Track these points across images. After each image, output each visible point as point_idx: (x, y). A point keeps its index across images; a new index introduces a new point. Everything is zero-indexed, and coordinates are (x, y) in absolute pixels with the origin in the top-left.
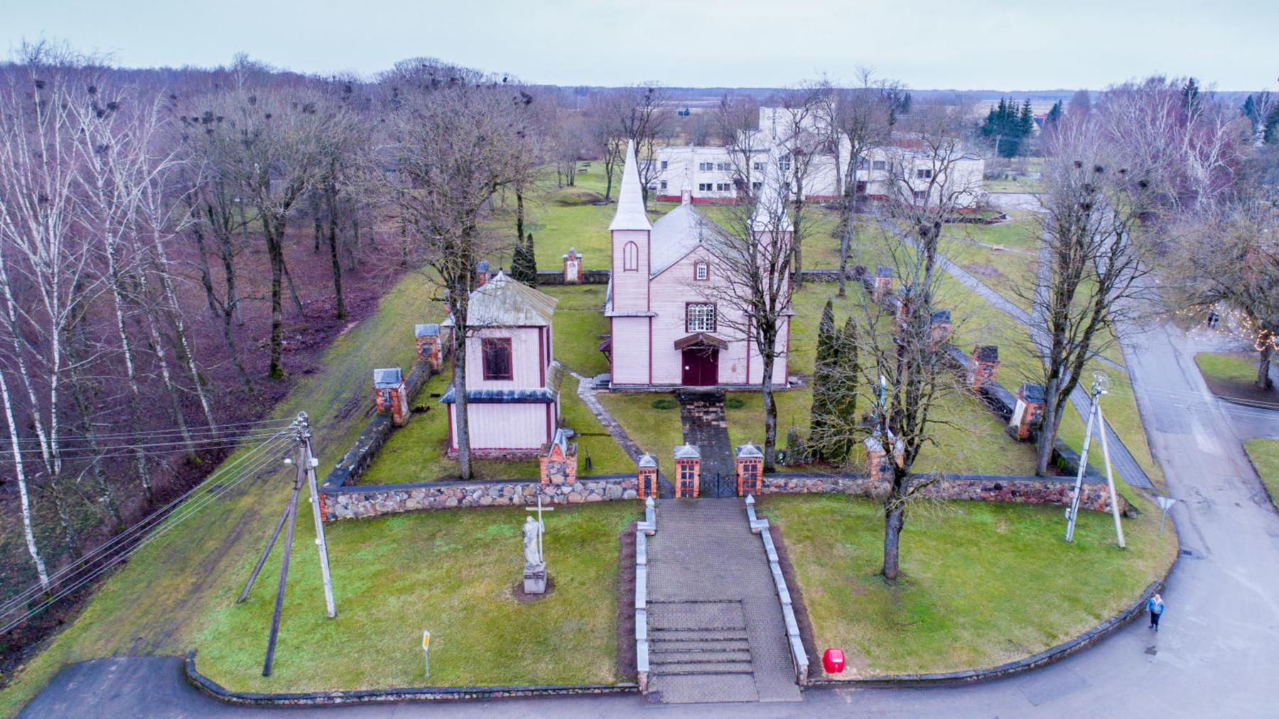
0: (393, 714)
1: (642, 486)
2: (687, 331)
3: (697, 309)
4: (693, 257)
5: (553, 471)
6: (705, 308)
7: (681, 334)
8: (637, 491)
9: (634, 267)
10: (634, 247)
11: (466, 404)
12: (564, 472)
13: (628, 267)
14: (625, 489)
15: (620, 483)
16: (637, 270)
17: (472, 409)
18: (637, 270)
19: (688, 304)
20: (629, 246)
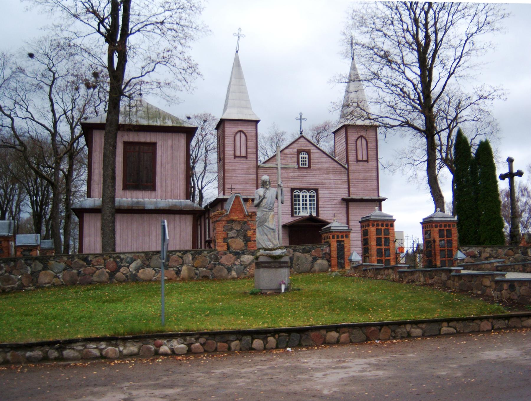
0: (94, 206)
1: (334, 254)
2: (292, 216)
3: (301, 194)
4: (296, 147)
5: (232, 234)
6: (308, 194)
7: (288, 219)
8: (329, 261)
9: (244, 154)
10: (243, 136)
11: (113, 216)
12: (245, 236)
13: (238, 154)
14: (315, 259)
15: (308, 252)
16: (246, 157)
17: (118, 217)
18: (246, 157)
19: (292, 190)
20: (238, 135)
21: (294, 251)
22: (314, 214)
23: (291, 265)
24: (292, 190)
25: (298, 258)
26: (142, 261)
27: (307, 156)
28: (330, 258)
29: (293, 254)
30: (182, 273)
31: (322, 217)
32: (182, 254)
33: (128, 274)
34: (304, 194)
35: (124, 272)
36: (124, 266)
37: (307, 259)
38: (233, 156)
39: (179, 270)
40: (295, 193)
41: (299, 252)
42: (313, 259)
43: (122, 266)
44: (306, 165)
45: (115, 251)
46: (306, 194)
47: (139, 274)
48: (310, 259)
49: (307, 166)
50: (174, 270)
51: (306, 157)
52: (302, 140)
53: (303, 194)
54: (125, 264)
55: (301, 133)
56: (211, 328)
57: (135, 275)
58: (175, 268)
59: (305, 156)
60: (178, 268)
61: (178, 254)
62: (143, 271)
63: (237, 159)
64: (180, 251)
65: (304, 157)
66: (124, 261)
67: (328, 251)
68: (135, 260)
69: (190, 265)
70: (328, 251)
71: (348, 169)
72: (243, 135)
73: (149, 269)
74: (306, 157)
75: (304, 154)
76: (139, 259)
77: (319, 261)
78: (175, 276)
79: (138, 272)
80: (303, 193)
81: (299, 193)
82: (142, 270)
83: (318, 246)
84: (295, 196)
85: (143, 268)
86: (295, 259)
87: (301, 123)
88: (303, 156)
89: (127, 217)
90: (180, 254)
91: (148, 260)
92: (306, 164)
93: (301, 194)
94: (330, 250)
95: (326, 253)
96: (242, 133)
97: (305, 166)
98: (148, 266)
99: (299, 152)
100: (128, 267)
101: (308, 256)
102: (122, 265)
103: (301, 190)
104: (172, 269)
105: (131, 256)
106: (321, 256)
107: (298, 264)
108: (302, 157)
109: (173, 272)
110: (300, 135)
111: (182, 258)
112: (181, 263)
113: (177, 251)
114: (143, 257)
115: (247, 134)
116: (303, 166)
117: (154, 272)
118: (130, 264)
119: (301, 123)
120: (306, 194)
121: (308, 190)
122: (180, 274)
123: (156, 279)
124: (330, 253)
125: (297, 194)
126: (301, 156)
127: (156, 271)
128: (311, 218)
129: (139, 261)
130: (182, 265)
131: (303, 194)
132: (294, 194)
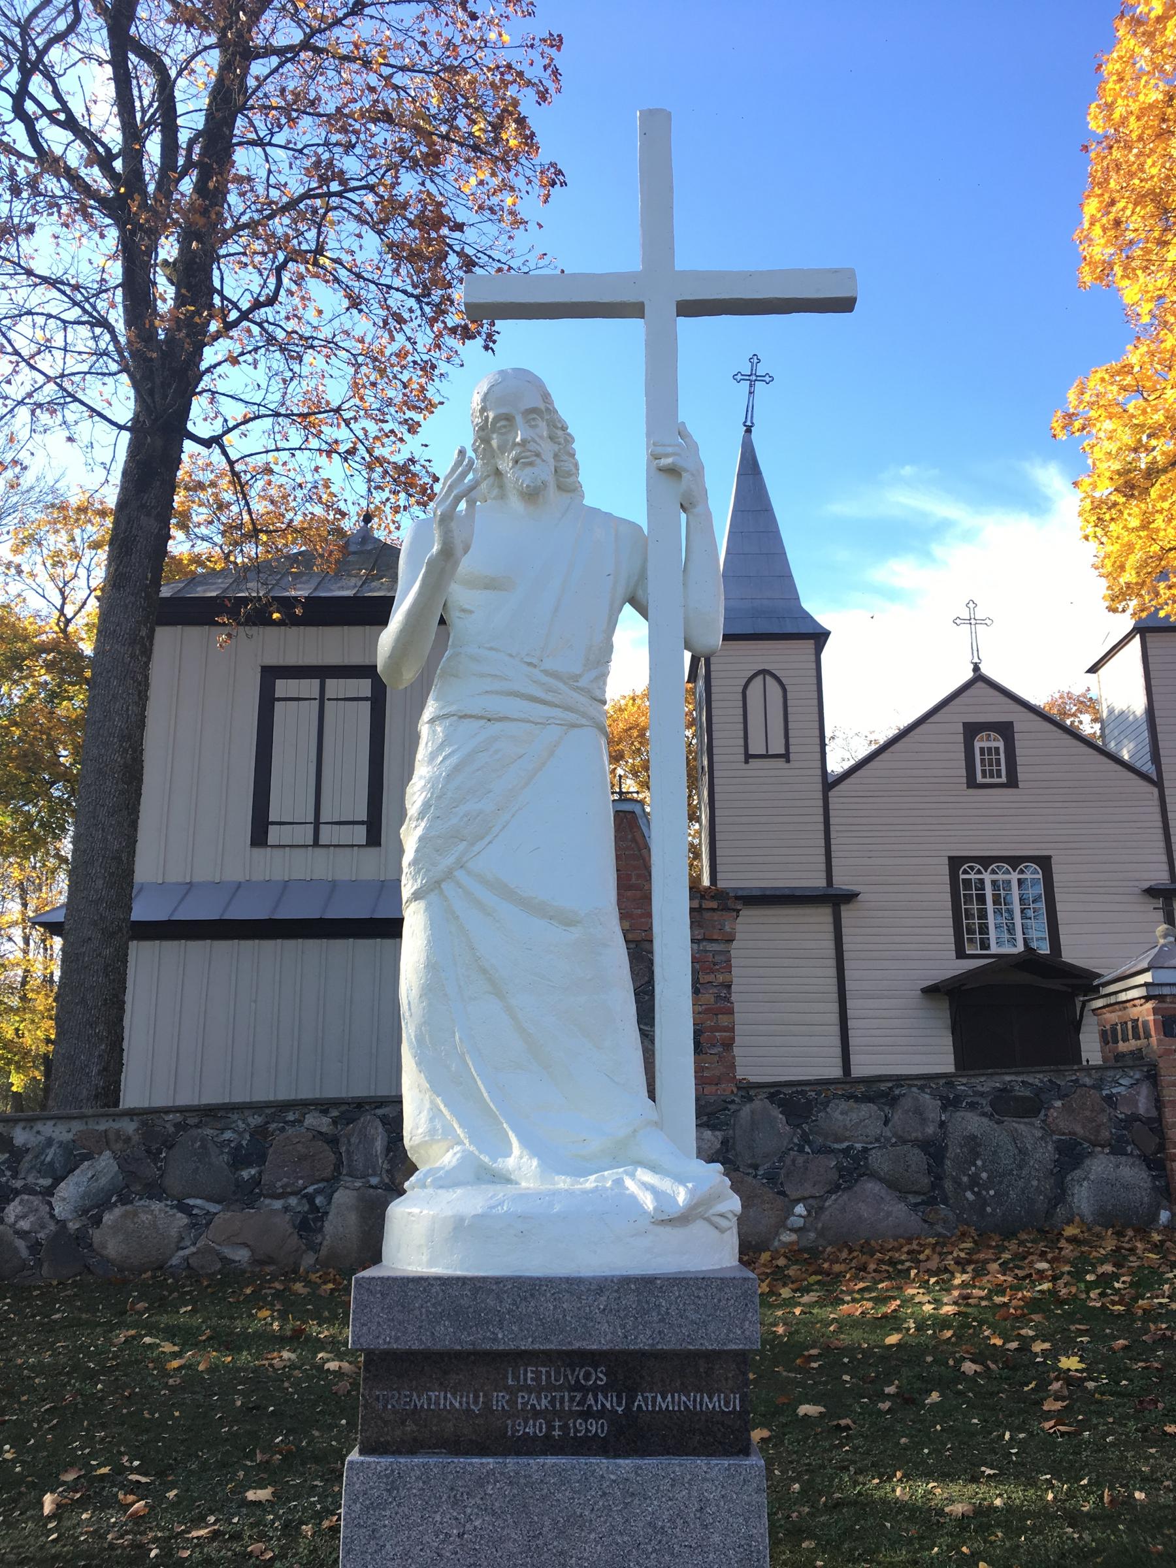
2: (961, 954)
3: (987, 877)
6: (1014, 877)
13: (756, 748)
19: (955, 863)
21: (944, 1108)
22: (1044, 949)
23: (934, 1186)
24: (955, 863)
25: (973, 1144)
26: (123, 1162)
27: (1001, 745)
28: (1162, 1147)
29: (942, 1124)
30: (328, 1227)
31: (1073, 954)
32: (335, 1122)
33: (41, 1235)
34: (1000, 877)
35: (24, 1225)
36: (29, 1190)
37: (1022, 1152)
38: (742, 758)
39: (314, 1208)
40: (965, 872)
41: (972, 1106)
42: (1061, 1148)
43: (17, 1193)
44: (999, 776)
45: (116, 1104)
46: (1006, 877)
47: (97, 1235)
48: (1045, 1154)
49: (1004, 779)
50: (286, 1209)
51: (997, 749)
52: (980, 684)
53: (994, 877)
54: (31, 1179)
55: (976, 668)
56: (710, 1348)
57: (81, 1239)
58: (293, 1201)
59: (994, 744)
60: (310, 1199)
61: (313, 1120)
62: (125, 1216)
63: (754, 763)
64: (323, 1106)
65: (990, 749)
66: (25, 1164)
67: (1143, 1105)
68: (88, 1157)
69: (374, 1181)
70: (1143, 1105)
71: (1158, 783)
72: (772, 684)
73: (156, 1206)
74: (997, 749)
75: (988, 740)
76: (108, 1153)
77: (1100, 1166)
78: (294, 1241)
79: (97, 1221)
80: (993, 872)
81: (979, 872)
82: (118, 1211)
83: (95, 537)
84: (967, 883)
85: (124, 1200)
86: (954, 1150)
87: (974, 636)
88: (985, 744)
89: (171, 949)
90: (323, 1123)
91: (154, 1155)
92: (999, 771)
93: (987, 877)
94: (1159, 1103)
95: (1135, 1118)
96: (768, 677)
97: (996, 780)
98: (155, 1191)
99: (972, 730)
100: (49, 1192)
101: (1028, 1130)
102: (18, 1184)
103: (986, 862)
104: (278, 1204)
105: (67, 1137)
106: (1105, 1134)
107: (974, 1181)
108: (982, 749)
109: (284, 1223)
110: (969, 675)
111: (333, 1141)
112: (328, 1172)
113: (304, 1105)
114: (128, 1139)
115: (784, 681)
116: (988, 780)
117: (182, 1219)
118: (58, 1180)
119: (974, 636)
120: (1006, 877)
121: (1014, 862)
122: (320, 1230)
123: (186, 1259)
124: (1160, 1119)
125: (973, 876)
126: (978, 745)
127: (190, 1215)
128: (1029, 961)
129: (106, 1164)
130: (332, 1182)
131: (994, 877)
132: (962, 877)
